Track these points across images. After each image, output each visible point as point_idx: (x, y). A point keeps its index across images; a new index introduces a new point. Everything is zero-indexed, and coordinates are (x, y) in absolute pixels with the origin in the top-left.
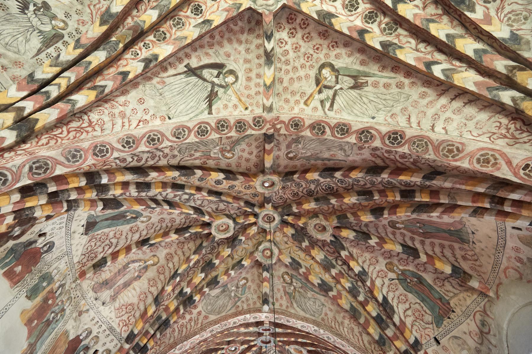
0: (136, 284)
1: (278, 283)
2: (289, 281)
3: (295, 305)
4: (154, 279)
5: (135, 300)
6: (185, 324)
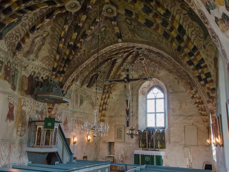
0: (43, 47)
1: (124, 25)
2: (130, 23)
3: (136, 35)
4: (51, 43)
5: (48, 54)
6: (79, 57)
